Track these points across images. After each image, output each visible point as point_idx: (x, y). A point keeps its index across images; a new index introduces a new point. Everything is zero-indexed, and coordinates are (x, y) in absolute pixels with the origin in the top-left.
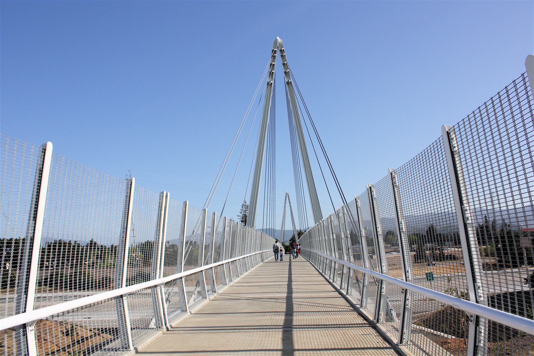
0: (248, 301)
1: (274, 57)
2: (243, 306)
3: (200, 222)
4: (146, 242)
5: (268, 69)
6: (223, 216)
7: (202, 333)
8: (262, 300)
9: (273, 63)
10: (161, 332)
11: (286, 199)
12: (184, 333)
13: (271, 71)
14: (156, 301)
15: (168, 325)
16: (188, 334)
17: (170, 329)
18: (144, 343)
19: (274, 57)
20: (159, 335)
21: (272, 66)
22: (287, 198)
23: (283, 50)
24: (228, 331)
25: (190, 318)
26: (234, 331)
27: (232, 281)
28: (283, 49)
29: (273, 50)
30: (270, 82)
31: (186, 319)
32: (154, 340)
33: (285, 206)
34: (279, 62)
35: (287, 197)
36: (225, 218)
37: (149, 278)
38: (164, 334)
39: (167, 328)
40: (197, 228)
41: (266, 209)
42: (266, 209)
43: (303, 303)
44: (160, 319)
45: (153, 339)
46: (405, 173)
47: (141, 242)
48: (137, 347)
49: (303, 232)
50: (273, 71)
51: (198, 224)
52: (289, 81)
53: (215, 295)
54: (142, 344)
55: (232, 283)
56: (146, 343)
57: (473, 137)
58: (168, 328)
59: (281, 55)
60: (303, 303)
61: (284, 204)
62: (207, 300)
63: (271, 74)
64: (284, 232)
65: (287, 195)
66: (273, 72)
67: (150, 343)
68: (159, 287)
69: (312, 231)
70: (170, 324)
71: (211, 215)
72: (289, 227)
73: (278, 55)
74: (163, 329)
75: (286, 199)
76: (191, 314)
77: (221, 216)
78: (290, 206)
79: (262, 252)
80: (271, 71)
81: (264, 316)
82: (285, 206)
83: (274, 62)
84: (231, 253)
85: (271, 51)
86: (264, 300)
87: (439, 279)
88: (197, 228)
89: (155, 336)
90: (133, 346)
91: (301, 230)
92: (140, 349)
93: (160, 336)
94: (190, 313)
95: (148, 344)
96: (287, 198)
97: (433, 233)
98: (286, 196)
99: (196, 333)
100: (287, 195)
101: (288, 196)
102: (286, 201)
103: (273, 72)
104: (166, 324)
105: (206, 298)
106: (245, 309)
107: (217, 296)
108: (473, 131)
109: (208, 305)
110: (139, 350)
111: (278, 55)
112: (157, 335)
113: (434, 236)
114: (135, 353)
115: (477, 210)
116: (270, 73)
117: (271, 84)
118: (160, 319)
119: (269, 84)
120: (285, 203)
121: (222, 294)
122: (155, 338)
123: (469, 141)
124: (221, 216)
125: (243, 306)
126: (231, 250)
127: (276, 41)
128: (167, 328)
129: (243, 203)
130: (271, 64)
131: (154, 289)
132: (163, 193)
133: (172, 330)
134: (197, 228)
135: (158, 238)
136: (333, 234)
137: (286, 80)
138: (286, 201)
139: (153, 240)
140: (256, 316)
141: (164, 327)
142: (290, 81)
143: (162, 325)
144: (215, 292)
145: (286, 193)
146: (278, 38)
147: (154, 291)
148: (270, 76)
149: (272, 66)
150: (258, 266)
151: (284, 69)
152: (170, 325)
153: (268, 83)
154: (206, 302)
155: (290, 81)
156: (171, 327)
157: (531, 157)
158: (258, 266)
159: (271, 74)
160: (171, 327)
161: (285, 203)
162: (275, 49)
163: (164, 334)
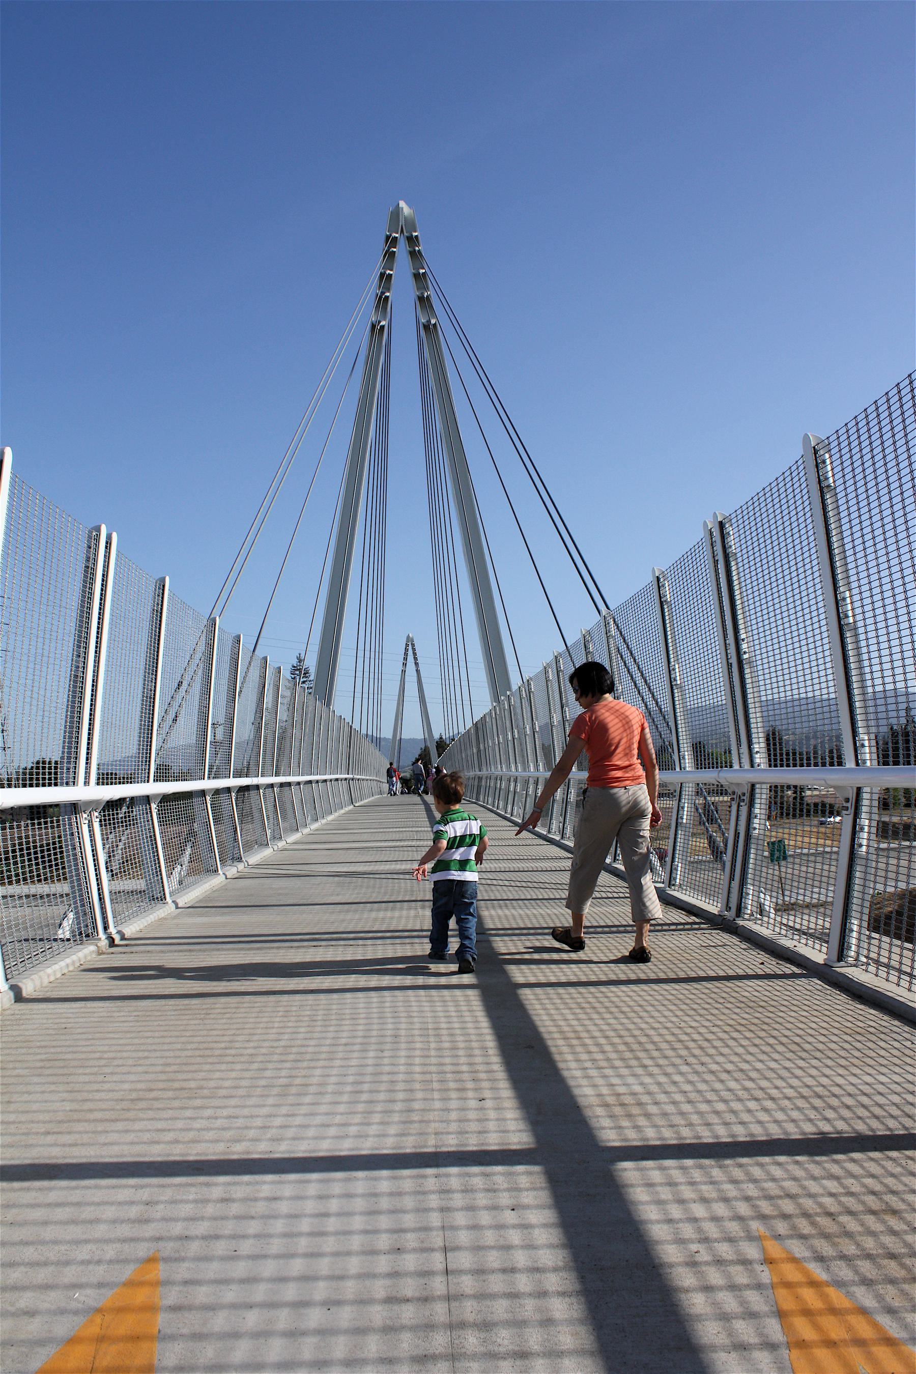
0: (337, 879)
1: (390, 256)
2: (330, 890)
3: (198, 655)
4: (38, 763)
5: (372, 287)
6: (260, 653)
7: (218, 950)
8: (377, 876)
9: (388, 272)
10: (92, 948)
11: (406, 654)
12: (162, 952)
13: (383, 293)
14: (75, 855)
15: (112, 930)
16: (176, 954)
17: (117, 942)
18: (41, 974)
19: (390, 256)
20: (85, 957)
21: (385, 279)
22: (410, 652)
23: (416, 236)
24: (296, 944)
25: (175, 917)
26: (315, 943)
27: (281, 838)
28: (415, 234)
29: (388, 237)
30: (380, 322)
31: (165, 919)
32: (71, 968)
33: (404, 672)
34: (402, 269)
35: (410, 648)
36: (265, 659)
37: (56, 779)
38: (100, 953)
39: (111, 940)
40: (190, 672)
41: (360, 660)
42: (360, 660)
43: (495, 882)
44: (88, 910)
45: (67, 966)
46: (758, 560)
47: (23, 766)
48: (20, 984)
49: (448, 742)
50: (388, 294)
51: (193, 666)
52: (429, 321)
53: (241, 866)
54: (33, 977)
55: (281, 844)
56: (49, 976)
57: (902, 493)
58: (113, 940)
59: (411, 249)
60: (495, 882)
61: (401, 667)
62: (219, 877)
63: (382, 302)
64: (398, 743)
65: (410, 643)
66: (387, 298)
67: (59, 975)
68: (85, 816)
69: (489, 725)
70: (119, 928)
71: (229, 643)
72: (413, 730)
73: (401, 250)
74: (100, 939)
75: (406, 654)
76: (177, 907)
77: (254, 650)
78: (418, 671)
79: (351, 776)
80: (383, 293)
81: (393, 909)
82: (404, 672)
83: (391, 270)
84: (278, 761)
85: (383, 238)
86: (383, 876)
87: (812, 858)
88: (190, 672)
89: (74, 957)
90: (7, 980)
91: (441, 738)
92: (29, 988)
93: (89, 958)
94: (173, 906)
95: (52, 978)
96: (410, 652)
97: (781, 749)
98: (407, 645)
99: (200, 950)
100: (410, 643)
101: (413, 645)
102: (405, 659)
103: (387, 298)
104: (106, 928)
105: (216, 871)
106: (332, 895)
107: (246, 870)
108: (904, 480)
109: (223, 889)
110: (25, 994)
111: (401, 250)
112: (81, 954)
113: (781, 755)
114: (13, 1001)
115: (899, 692)
116: (381, 297)
117: (383, 327)
118: (88, 910)
119: (376, 330)
120: (405, 665)
121: (257, 866)
122: (73, 963)
123: (885, 514)
124: (254, 650)
125: (330, 890)
126: (279, 755)
127: (397, 211)
128: (111, 940)
129: (295, 662)
130: (382, 275)
131: (70, 819)
132: (98, 529)
133: (126, 945)
134: (178, 704)
135: (81, 665)
136: (562, 707)
137: (423, 320)
138: (405, 659)
139: (56, 757)
140: (371, 910)
141: (102, 935)
142: (433, 321)
143: (95, 927)
144: (240, 859)
145: (408, 636)
146: (402, 204)
147: (70, 824)
148: (377, 307)
149: (385, 279)
150: (342, 811)
151: (418, 289)
152: (119, 932)
153: (373, 327)
154: (216, 881)
155: (433, 321)
156: (123, 938)
157: (913, 642)
158: (342, 811)
159: (382, 302)
160: (123, 938)
161: (405, 665)
162: (394, 235)
163: (100, 953)
